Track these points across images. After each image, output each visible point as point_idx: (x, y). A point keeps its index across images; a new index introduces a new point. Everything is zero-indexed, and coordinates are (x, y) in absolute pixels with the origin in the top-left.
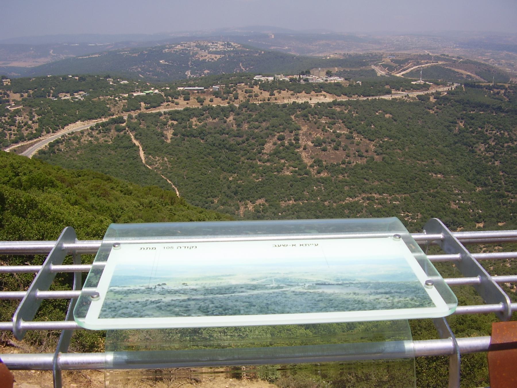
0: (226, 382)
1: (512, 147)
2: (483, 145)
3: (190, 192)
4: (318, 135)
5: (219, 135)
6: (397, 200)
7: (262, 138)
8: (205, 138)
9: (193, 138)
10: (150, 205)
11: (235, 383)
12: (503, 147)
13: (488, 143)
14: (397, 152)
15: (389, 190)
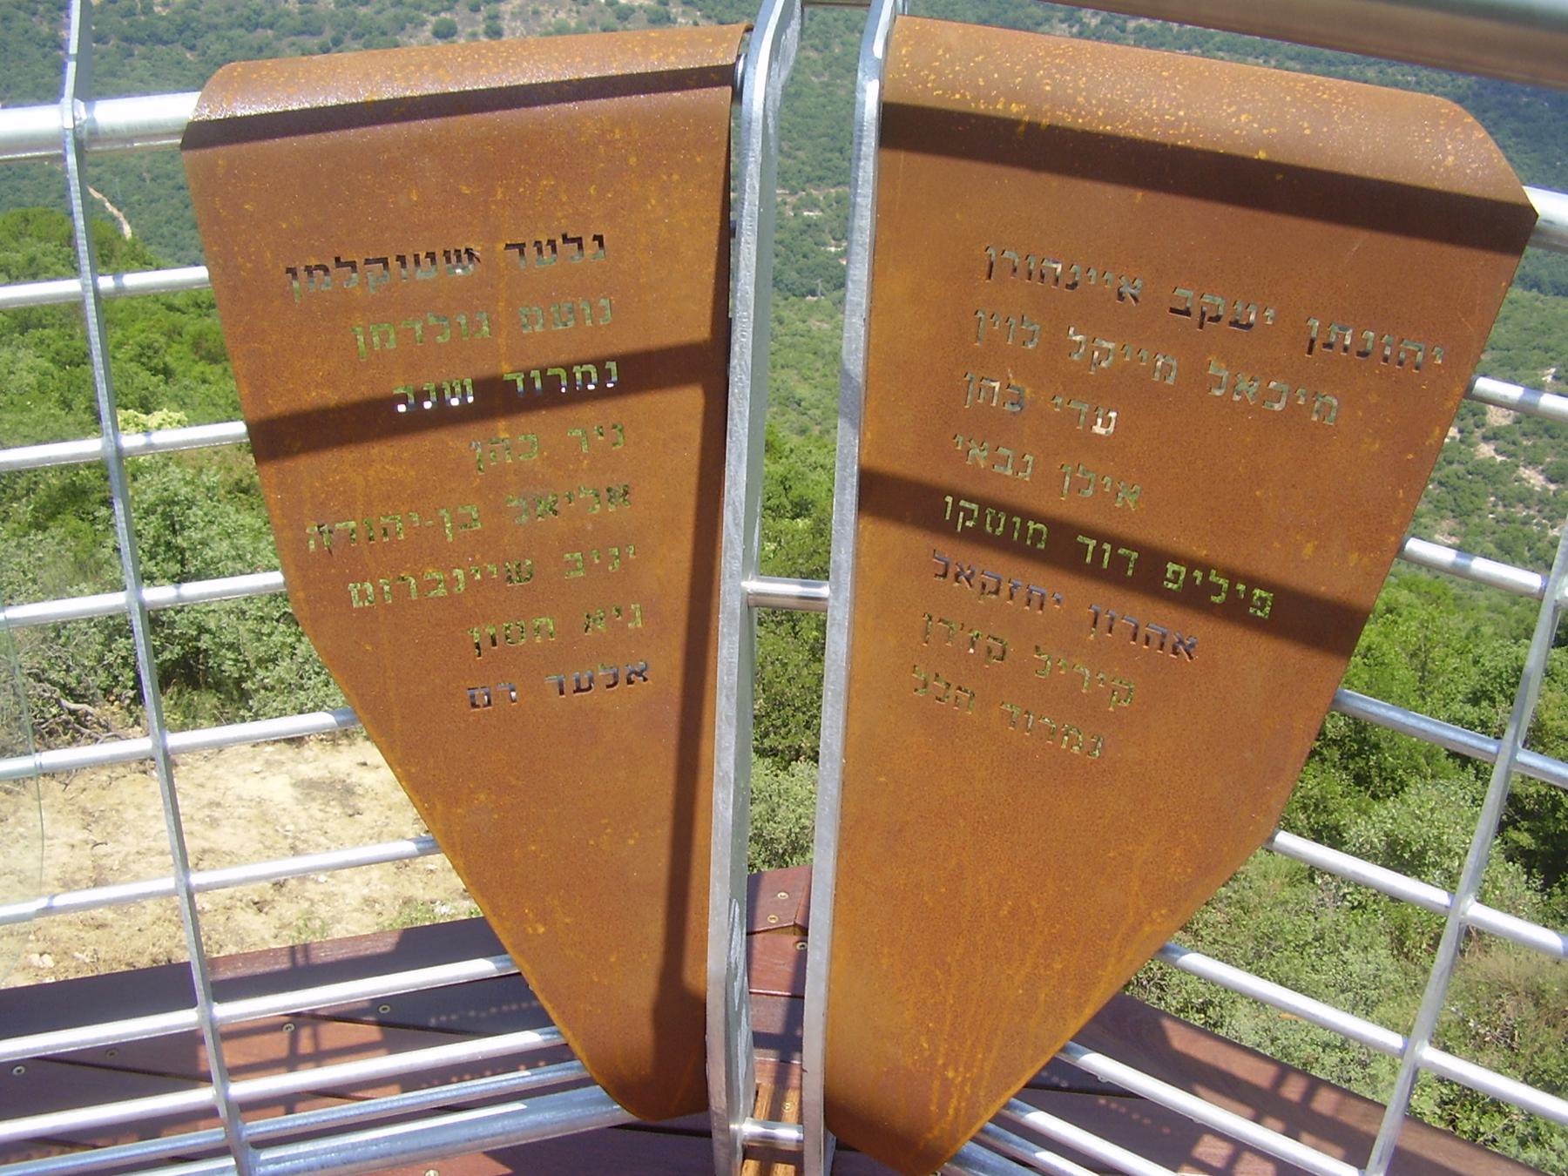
0: (254, 758)
1: (1151, 30)
2: (1065, 26)
3: (168, 222)
4: (562, 15)
5: (241, 31)
6: (814, 205)
7: (384, 34)
8: (199, 43)
9: (159, 48)
10: (32, 270)
11: (282, 758)
12: (1123, 31)
13: (1079, 21)
14: (807, 58)
15: (788, 176)
